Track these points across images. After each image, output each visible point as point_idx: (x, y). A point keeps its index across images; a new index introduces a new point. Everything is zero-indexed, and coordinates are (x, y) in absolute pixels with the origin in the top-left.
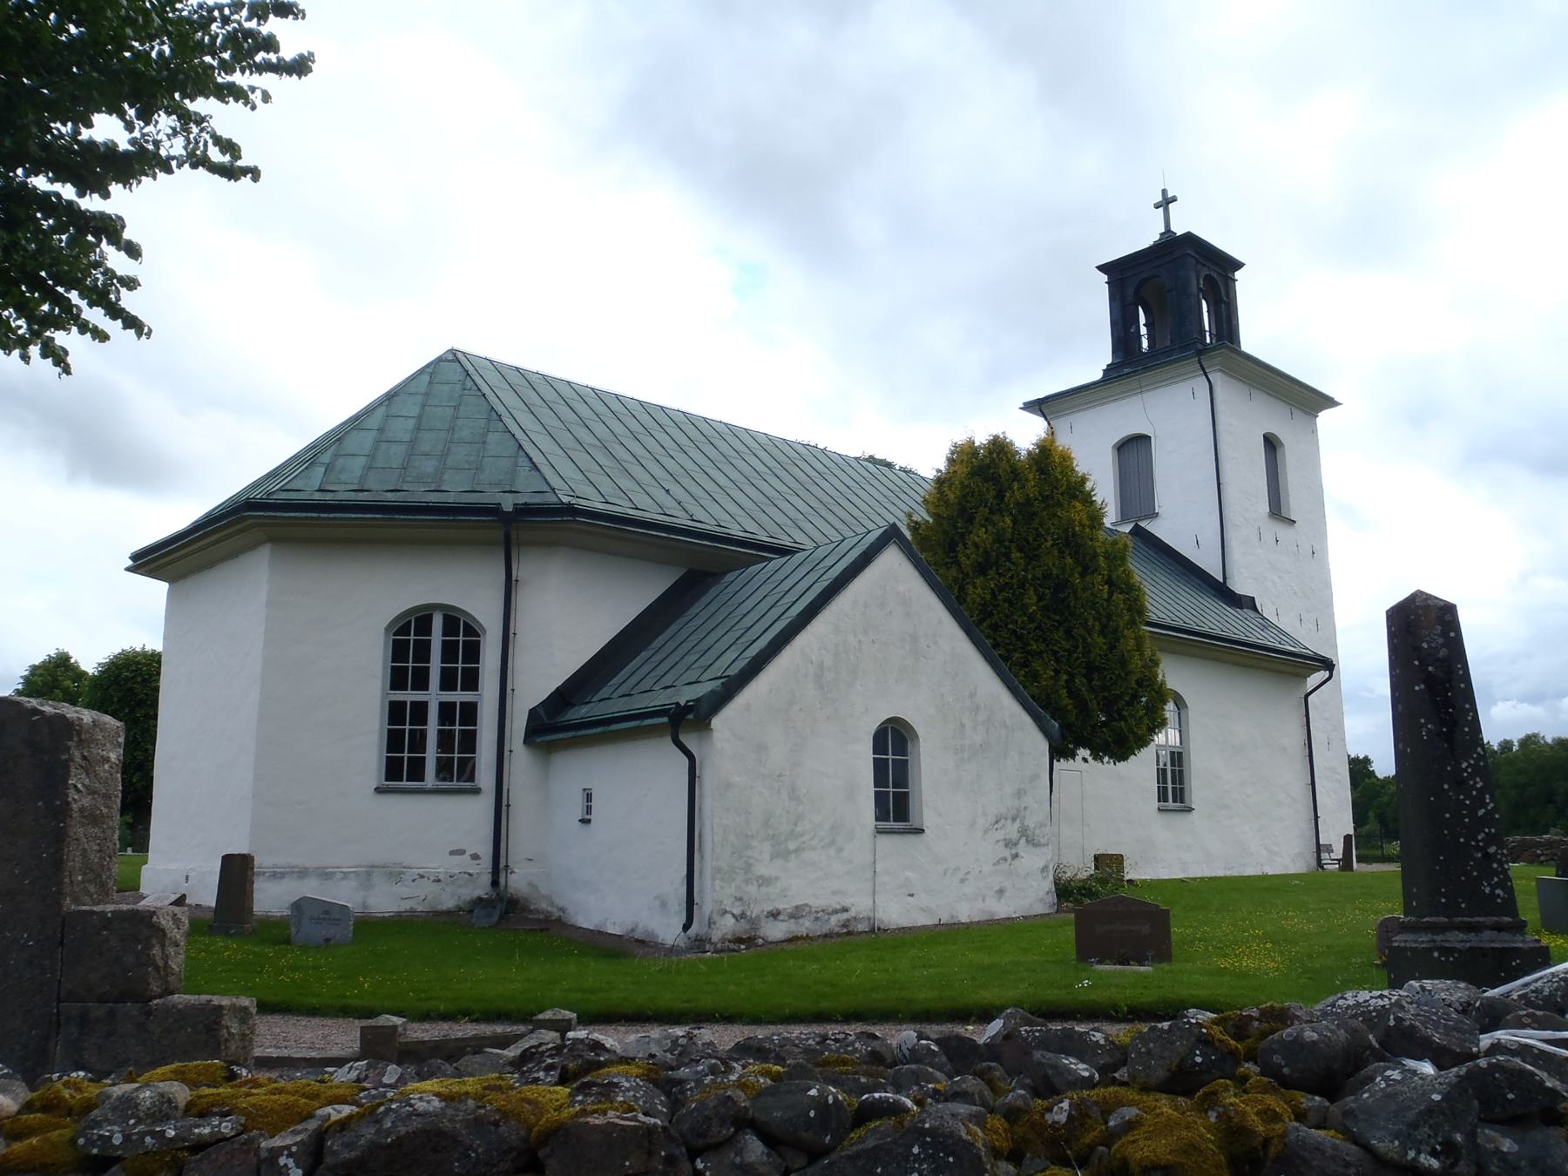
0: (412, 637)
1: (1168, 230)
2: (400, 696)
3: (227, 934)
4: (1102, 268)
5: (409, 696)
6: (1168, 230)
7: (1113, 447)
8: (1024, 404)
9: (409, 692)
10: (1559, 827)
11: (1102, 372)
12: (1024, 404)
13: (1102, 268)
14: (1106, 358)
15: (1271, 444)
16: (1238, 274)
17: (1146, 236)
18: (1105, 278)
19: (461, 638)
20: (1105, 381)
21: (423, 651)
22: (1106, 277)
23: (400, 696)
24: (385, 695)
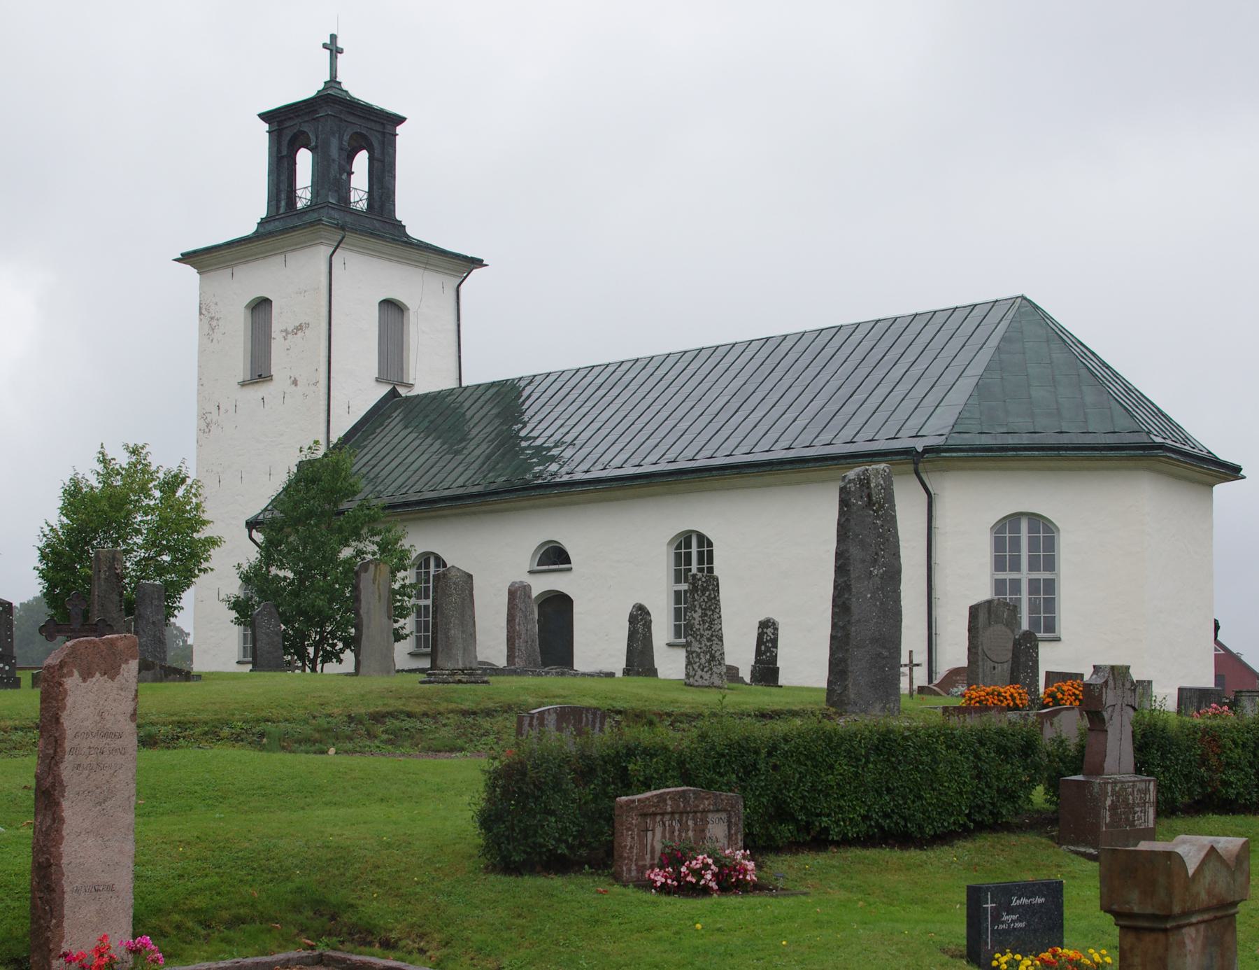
0: (1041, 535)
1: (333, 82)
2: (1001, 575)
3: (37, 799)
4: (265, 117)
5: (1042, 575)
6: (333, 82)
7: (247, 307)
8: (182, 255)
9: (1042, 572)
10: (653, 787)
11: (256, 225)
12: (182, 255)
13: (265, 117)
14: (261, 209)
15: (392, 308)
16: (399, 129)
17: (305, 87)
18: (266, 126)
19: (1041, 535)
20: (271, 234)
21: (1016, 543)
22: (267, 125)
23: (1001, 575)
24: (1058, 575)
